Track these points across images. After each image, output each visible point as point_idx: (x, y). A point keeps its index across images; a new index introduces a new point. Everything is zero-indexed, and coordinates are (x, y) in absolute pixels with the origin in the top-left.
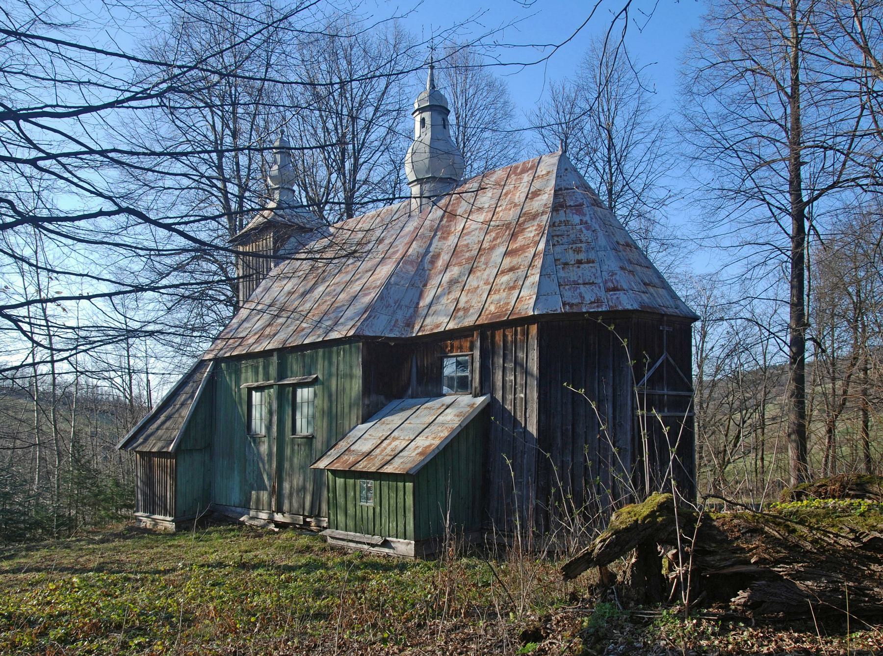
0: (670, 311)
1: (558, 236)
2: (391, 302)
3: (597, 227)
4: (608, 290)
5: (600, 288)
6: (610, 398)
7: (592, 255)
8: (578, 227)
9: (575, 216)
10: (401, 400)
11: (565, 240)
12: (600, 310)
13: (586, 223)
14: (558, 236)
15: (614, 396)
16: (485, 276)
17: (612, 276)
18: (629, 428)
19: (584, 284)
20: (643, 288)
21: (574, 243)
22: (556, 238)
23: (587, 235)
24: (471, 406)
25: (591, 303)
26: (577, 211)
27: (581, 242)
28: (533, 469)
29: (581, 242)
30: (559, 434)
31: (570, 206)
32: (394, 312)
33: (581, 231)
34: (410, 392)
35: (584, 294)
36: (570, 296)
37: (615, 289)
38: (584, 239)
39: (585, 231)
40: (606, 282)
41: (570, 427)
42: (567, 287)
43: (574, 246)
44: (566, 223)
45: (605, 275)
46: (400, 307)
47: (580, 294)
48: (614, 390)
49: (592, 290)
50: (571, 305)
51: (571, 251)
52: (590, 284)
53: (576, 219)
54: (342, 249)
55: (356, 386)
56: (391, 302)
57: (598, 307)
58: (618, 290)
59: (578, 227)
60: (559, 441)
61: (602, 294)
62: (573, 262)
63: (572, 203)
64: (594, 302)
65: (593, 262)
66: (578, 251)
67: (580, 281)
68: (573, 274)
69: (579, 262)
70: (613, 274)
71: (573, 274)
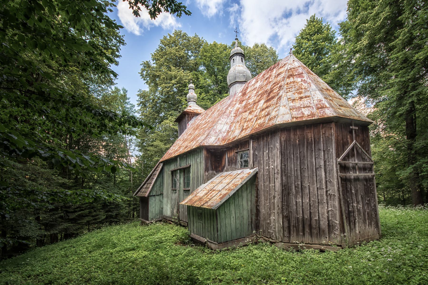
0: (356, 118)
1: (289, 88)
2: (217, 131)
3: (310, 81)
4: (318, 108)
5: (313, 108)
6: (323, 167)
7: (307, 94)
8: (300, 83)
9: (298, 79)
10: (221, 173)
11: (293, 89)
12: (313, 118)
13: (305, 80)
14: (289, 88)
15: (325, 165)
16: (255, 114)
17: (320, 102)
18: (335, 183)
19: (304, 107)
20: (339, 107)
21: (298, 90)
22: (288, 89)
23: (305, 85)
24: (249, 174)
25: (308, 116)
26: (299, 76)
27: (302, 89)
28: (280, 206)
29: (302, 89)
30: (294, 187)
31: (296, 75)
32: (218, 135)
33: (302, 84)
34: (225, 168)
35: (304, 112)
36: (295, 113)
37: (322, 108)
38: (303, 87)
39: (304, 84)
40: (317, 105)
41: (300, 183)
42: (294, 110)
43: (298, 91)
44: (294, 82)
45: (316, 102)
46: (221, 133)
47: (302, 112)
48: (325, 162)
49: (309, 110)
50: (297, 118)
51: (296, 94)
52: (307, 107)
53: (299, 80)
54: (412, 252)
55: (203, 165)
56: (217, 131)
57: (312, 117)
58: (324, 108)
59: (300, 83)
60: (294, 190)
61: (315, 110)
62: (298, 98)
63: (297, 74)
64: (310, 115)
65: (309, 97)
66: (300, 93)
67: (302, 106)
68: (297, 104)
69: (301, 98)
70: (321, 101)
71: (297, 104)
